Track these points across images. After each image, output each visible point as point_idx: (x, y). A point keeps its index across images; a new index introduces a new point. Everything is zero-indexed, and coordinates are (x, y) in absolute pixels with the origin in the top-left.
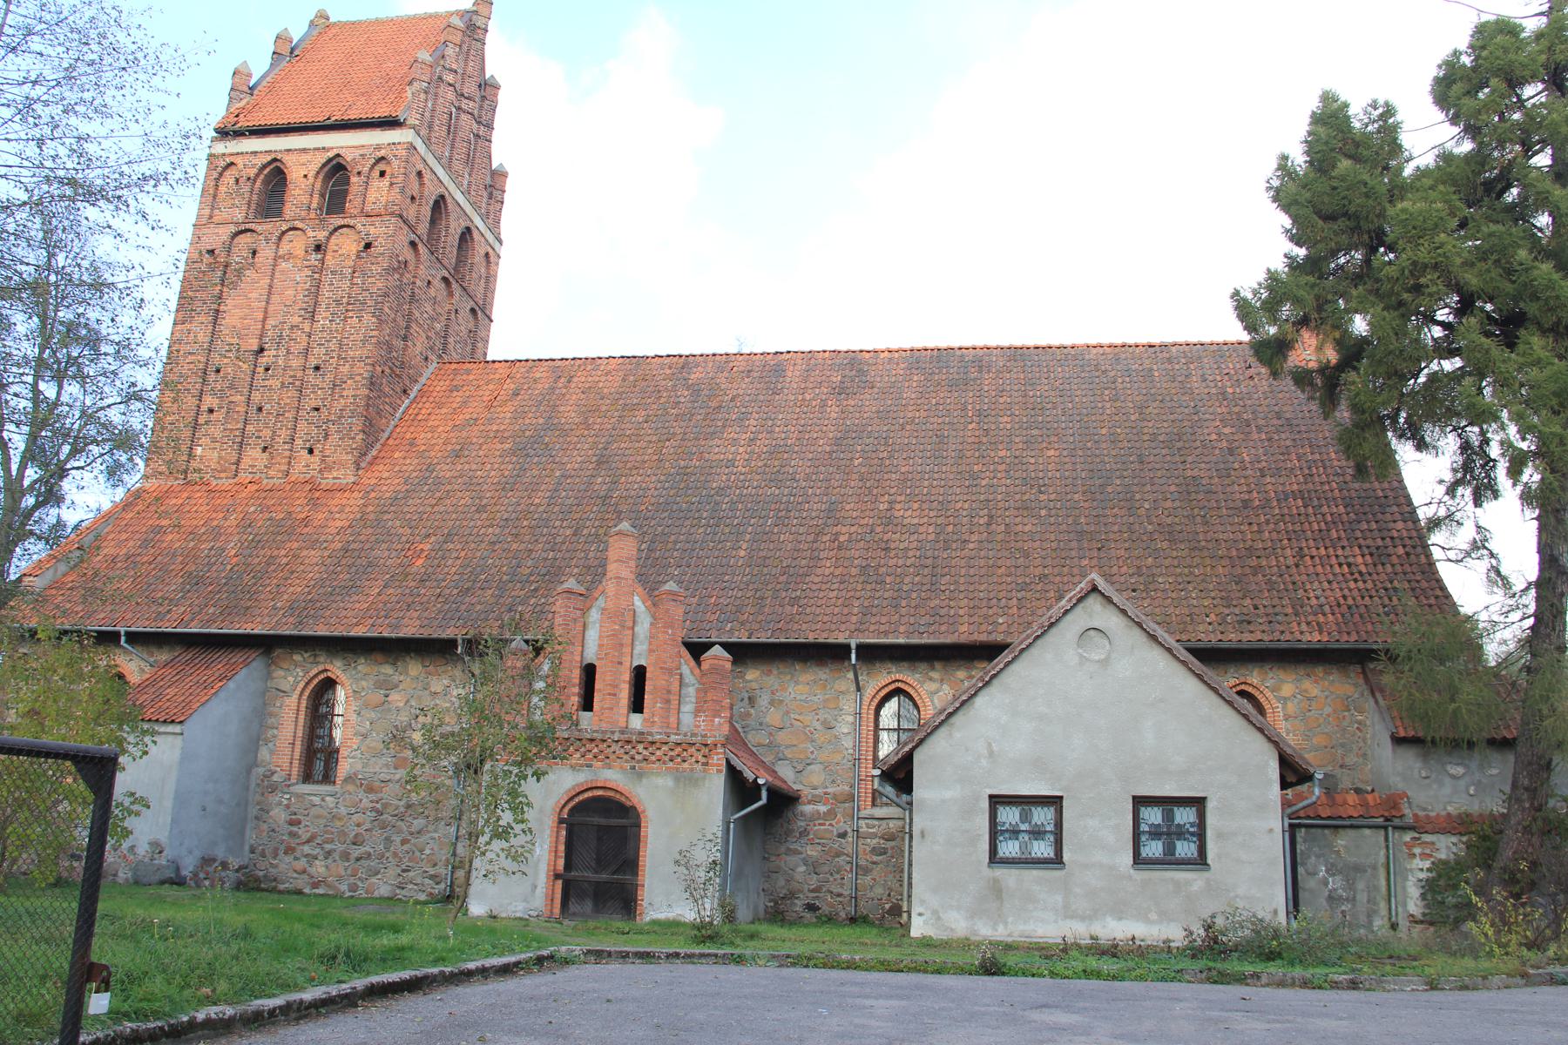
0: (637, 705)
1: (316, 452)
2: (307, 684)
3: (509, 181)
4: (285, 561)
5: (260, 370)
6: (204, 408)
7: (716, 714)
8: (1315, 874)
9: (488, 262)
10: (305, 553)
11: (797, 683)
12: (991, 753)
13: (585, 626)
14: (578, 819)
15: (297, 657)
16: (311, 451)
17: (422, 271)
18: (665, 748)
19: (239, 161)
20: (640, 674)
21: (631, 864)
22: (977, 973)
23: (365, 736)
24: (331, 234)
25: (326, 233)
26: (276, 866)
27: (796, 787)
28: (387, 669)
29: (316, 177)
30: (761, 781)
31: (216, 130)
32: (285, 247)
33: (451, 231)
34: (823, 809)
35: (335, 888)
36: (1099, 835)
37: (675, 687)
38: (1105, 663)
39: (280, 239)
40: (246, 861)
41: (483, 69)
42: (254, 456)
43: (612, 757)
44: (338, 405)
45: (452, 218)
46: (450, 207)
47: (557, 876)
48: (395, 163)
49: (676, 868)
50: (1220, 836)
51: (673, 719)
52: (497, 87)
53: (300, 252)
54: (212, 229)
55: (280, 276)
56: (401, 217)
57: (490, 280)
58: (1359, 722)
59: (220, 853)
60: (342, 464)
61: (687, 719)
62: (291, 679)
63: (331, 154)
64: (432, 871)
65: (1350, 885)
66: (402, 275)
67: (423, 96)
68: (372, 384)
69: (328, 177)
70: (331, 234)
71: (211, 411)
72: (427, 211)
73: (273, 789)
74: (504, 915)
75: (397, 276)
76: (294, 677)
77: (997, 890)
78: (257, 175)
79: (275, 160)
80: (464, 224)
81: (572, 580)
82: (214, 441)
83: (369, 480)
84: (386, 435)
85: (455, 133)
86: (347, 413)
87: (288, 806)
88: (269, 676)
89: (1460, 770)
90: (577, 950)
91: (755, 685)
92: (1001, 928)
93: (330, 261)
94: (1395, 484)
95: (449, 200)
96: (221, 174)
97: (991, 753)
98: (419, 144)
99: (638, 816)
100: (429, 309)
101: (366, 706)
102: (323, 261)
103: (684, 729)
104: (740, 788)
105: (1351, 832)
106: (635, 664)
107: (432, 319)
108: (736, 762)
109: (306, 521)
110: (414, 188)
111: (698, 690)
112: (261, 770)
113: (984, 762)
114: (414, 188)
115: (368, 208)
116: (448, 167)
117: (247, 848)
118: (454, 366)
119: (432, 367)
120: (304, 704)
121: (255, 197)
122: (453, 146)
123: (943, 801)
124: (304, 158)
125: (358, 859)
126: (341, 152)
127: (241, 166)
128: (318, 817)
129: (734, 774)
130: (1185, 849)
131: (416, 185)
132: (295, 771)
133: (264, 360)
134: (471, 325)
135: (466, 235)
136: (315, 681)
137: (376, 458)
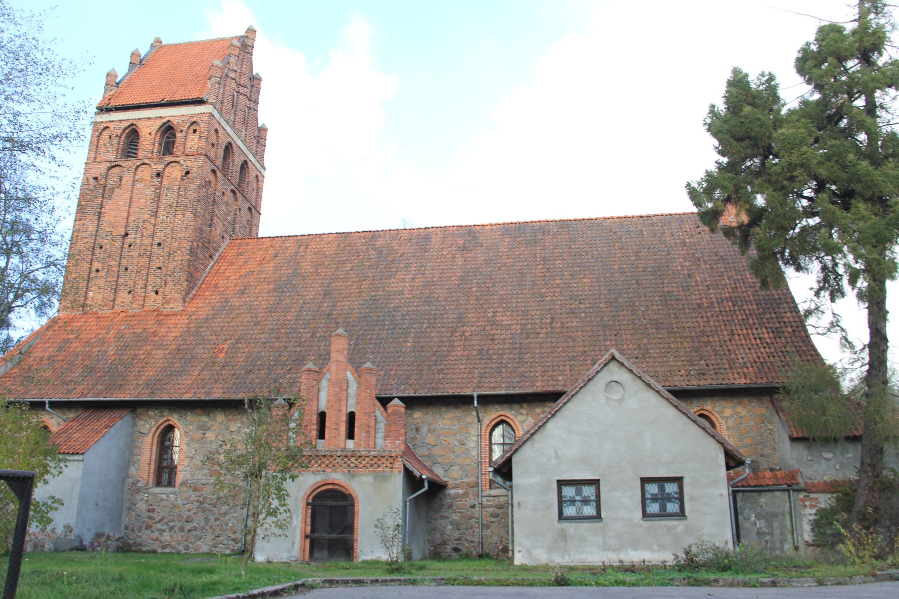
0: (351, 435)
1: (160, 293)
3: (268, 133)
4: (143, 357)
5: (126, 246)
6: (94, 269)
7: (397, 438)
9: (258, 180)
10: (154, 352)
11: (443, 419)
12: (557, 456)
13: (319, 390)
15: (151, 413)
16: (157, 293)
18: (367, 459)
19: (111, 126)
20: (351, 417)
21: (350, 528)
23: (192, 458)
24: (166, 166)
25: (163, 166)
27: (445, 479)
28: (204, 419)
29: (156, 134)
30: (424, 477)
31: (97, 108)
32: (139, 175)
33: (236, 163)
34: (461, 491)
36: (622, 500)
38: (621, 401)
39: (136, 170)
40: (122, 534)
41: (252, 70)
42: (123, 296)
43: (337, 465)
44: (172, 266)
46: (235, 149)
47: (306, 537)
48: (202, 125)
49: (376, 530)
50: (692, 499)
51: (372, 443)
52: (260, 80)
53: (148, 177)
54: (96, 165)
55: (136, 190)
56: (206, 155)
58: (770, 430)
59: (107, 530)
60: (176, 300)
61: (380, 442)
62: (148, 426)
63: (164, 121)
64: (233, 536)
65: (770, 525)
66: (207, 189)
67: (217, 86)
68: (192, 252)
70: (166, 166)
71: (98, 271)
72: (221, 152)
73: (138, 491)
74: (275, 561)
75: (204, 190)
76: (149, 426)
77: (563, 536)
78: (122, 134)
79: (132, 124)
81: (311, 363)
82: (100, 288)
83: (191, 308)
84: (201, 282)
85: (236, 107)
86: (177, 270)
87: (147, 501)
88: (135, 424)
89: (830, 455)
91: (419, 421)
92: (567, 558)
93: (166, 182)
94: (785, 291)
95: (234, 145)
96: (101, 134)
97: (557, 456)
99: (353, 500)
100: (224, 208)
101: (192, 440)
102: (161, 182)
103: (378, 448)
104: (412, 481)
105: (769, 494)
106: (349, 410)
107: (226, 214)
108: (409, 466)
109: (155, 334)
111: (386, 425)
113: (553, 461)
115: (187, 151)
116: (233, 127)
117: (123, 527)
118: (239, 241)
120: (156, 440)
121: (121, 146)
122: (235, 114)
124: (149, 123)
125: (189, 531)
126: (171, 119)
127: (112, 129)
128: (165, 506)
129: (408, 473)
130: (672, 507)
131: (215, 137)
133: (128, 241)
134: (249, 217)
136: (162, 427)
137: (195, 296)
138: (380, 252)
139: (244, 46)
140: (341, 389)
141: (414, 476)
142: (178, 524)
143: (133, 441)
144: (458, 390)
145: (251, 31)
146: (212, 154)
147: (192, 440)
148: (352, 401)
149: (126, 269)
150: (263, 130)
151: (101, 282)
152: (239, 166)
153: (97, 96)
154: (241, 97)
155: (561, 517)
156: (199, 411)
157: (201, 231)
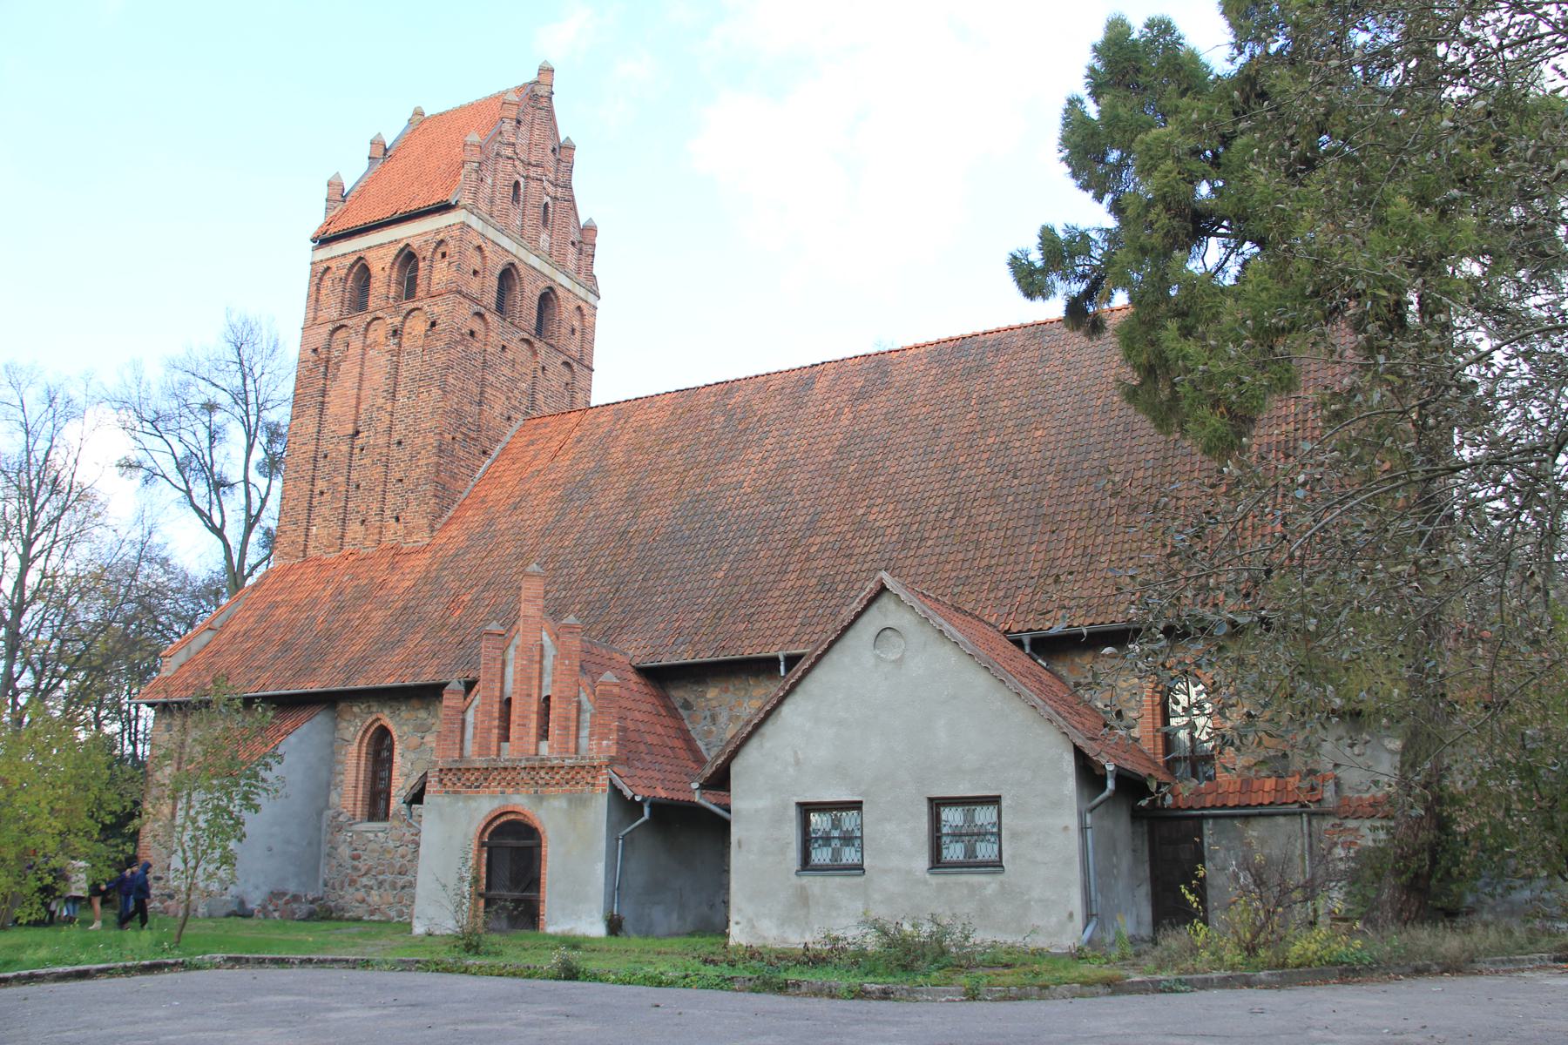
0: (544, 734)
2: (365, 732)
5: (357, 451)
6: (317, 491)
8: (1224, 869)
11: (751, 698)
12: (797, 762)
13: (504, 663)
14: (496, 842)
15: (356, 709)
16: (397, 519)
17: (494, 338)
19: (333, 264)
22: (558, 978)
24: (405, 318)
26: (341, 897)
28: (422, 714)
30: (638, 799)
32: (371, 336)
33: (528, 293)
35: (384, 914)
36: (895, 840)
37: (574, 713)
38: (899, 662)
39: (367, 330)
40: (321, 894)
41: (556, 134)
42: (355, 528)
44: (415, 475)
45: (525, 283)
46: (522, 273)
48: (452, 243)
50: (1015, 835)
51: (572, 745)
53: (382, 339)
54: (316, 330)
55: (368, 361)
56: (459, 292)
57: (586, 334)
59: (292, 887)
60: (420, 529)
63: (401, 245)
68: (440, 450)
69: (403, 266)
70: (405, 318)
71: (322, 493)
72: (493, 283)
75: (460, 348)
76: (354, 728)
77: (804, 898)
78: (348, 275)
79: (360, 258)
80: (542, 285)
81: (572, 617)
86: (422, 481)
88: (336, 727)
90: (219, 956)
91: (714, 703)
93: (406, 343)
95: (520, 267)
97: (797, 762)
98: (474, 222)
100: (507, 371)
101: (408, 748)
103: (582, 752)
105: (1264, 822)
106: (544, 695)
108: (618, 782)
110: (476, 262)
112: (331, 812)
113: (791, 770)
114: (476, 262)
119: (516, 426)
123: (756, 811)
124: (382, 252)
128: (373, 851)
129: (616, 792)
132: (359, 812)
133: (359, 442)
135: (547, 299)
138: (729, 415)
139: (536, 100)
140: (531, 661)
141: (625, 797)
142: (389, 877)
143: (333, 753)
144: (749, 650)
145: (547, 71)
146: (474, 286)
147: (408, 748)
148: (547, 680)
149: (358, 487)
150: (589, 231)
151: (325, 511)
152: (536, 299)
153: (315, 219)
154: (533, 184)
155: (806, 864)
156: (415, 702)
157: (459, 414)
